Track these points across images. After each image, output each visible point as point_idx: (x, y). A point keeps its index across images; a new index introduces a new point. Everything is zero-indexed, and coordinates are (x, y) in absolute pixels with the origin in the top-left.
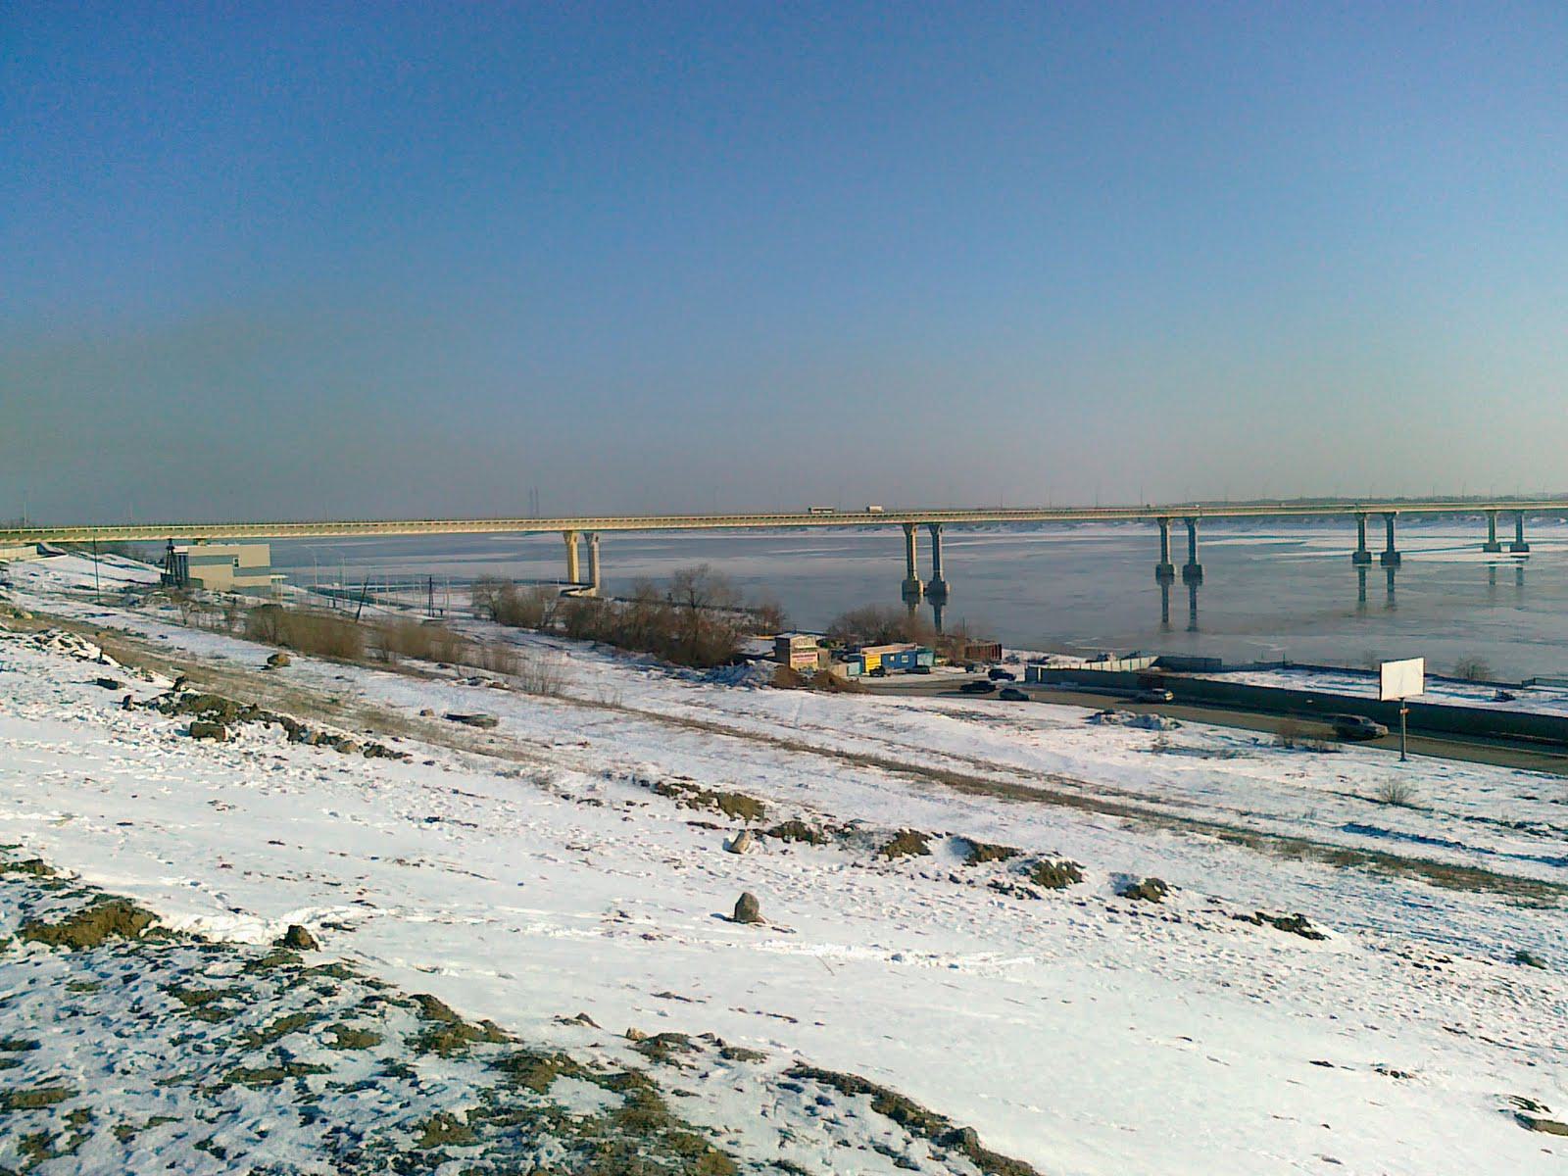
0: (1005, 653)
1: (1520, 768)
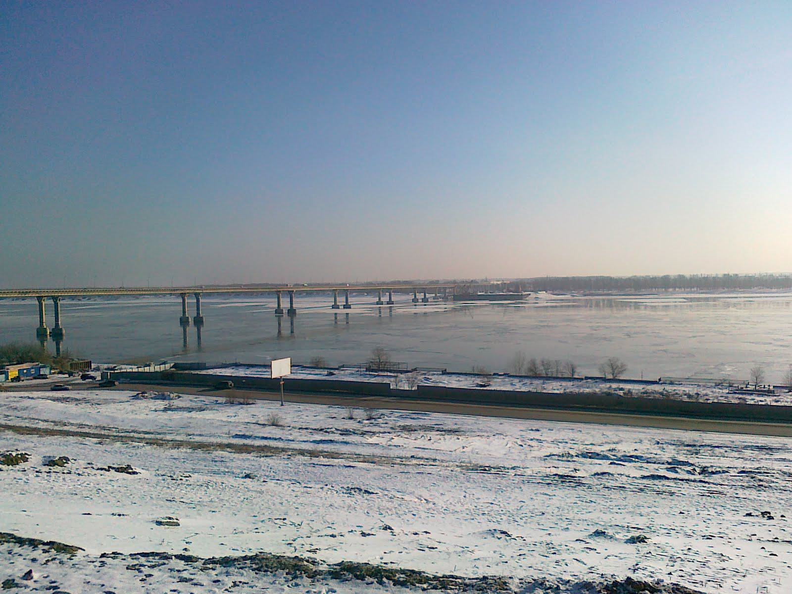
0: (93, 366)
1: (331, 405)
